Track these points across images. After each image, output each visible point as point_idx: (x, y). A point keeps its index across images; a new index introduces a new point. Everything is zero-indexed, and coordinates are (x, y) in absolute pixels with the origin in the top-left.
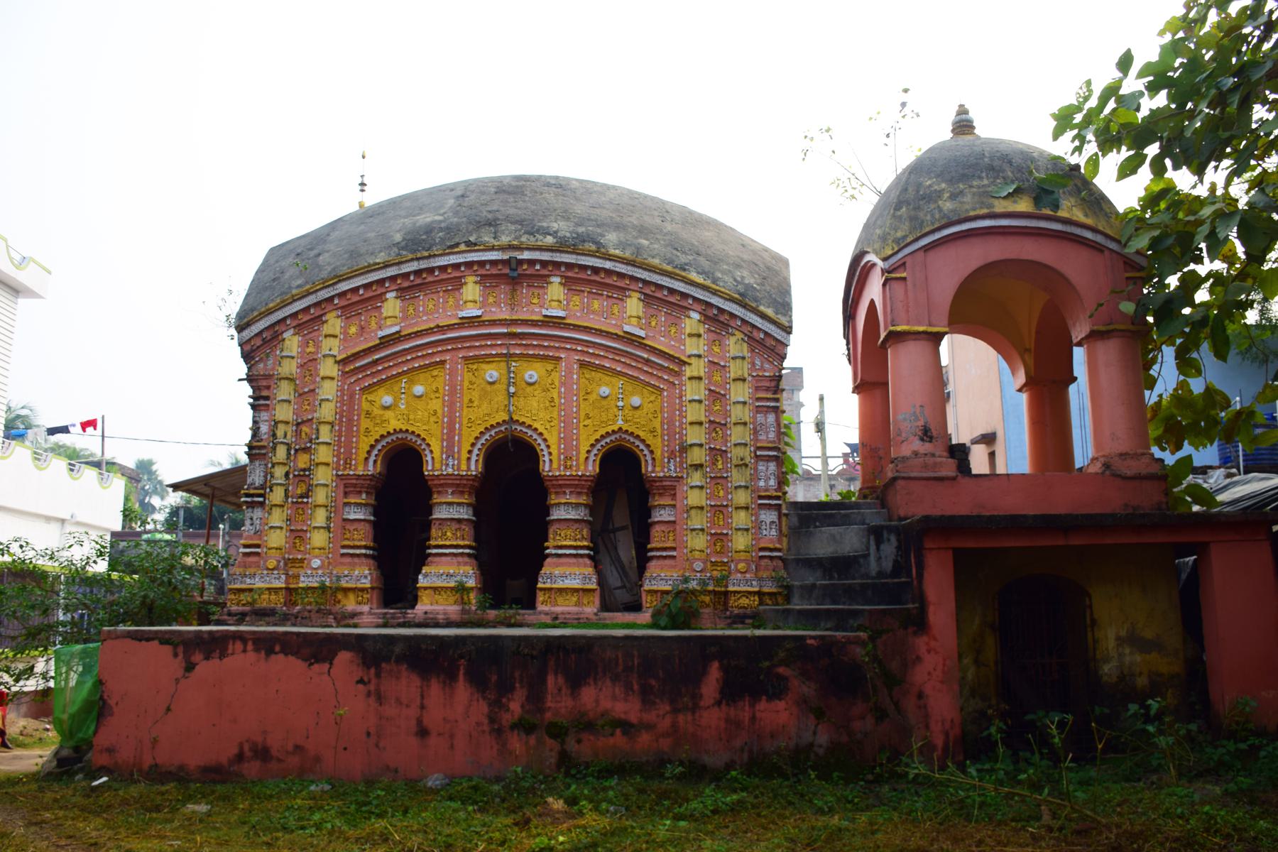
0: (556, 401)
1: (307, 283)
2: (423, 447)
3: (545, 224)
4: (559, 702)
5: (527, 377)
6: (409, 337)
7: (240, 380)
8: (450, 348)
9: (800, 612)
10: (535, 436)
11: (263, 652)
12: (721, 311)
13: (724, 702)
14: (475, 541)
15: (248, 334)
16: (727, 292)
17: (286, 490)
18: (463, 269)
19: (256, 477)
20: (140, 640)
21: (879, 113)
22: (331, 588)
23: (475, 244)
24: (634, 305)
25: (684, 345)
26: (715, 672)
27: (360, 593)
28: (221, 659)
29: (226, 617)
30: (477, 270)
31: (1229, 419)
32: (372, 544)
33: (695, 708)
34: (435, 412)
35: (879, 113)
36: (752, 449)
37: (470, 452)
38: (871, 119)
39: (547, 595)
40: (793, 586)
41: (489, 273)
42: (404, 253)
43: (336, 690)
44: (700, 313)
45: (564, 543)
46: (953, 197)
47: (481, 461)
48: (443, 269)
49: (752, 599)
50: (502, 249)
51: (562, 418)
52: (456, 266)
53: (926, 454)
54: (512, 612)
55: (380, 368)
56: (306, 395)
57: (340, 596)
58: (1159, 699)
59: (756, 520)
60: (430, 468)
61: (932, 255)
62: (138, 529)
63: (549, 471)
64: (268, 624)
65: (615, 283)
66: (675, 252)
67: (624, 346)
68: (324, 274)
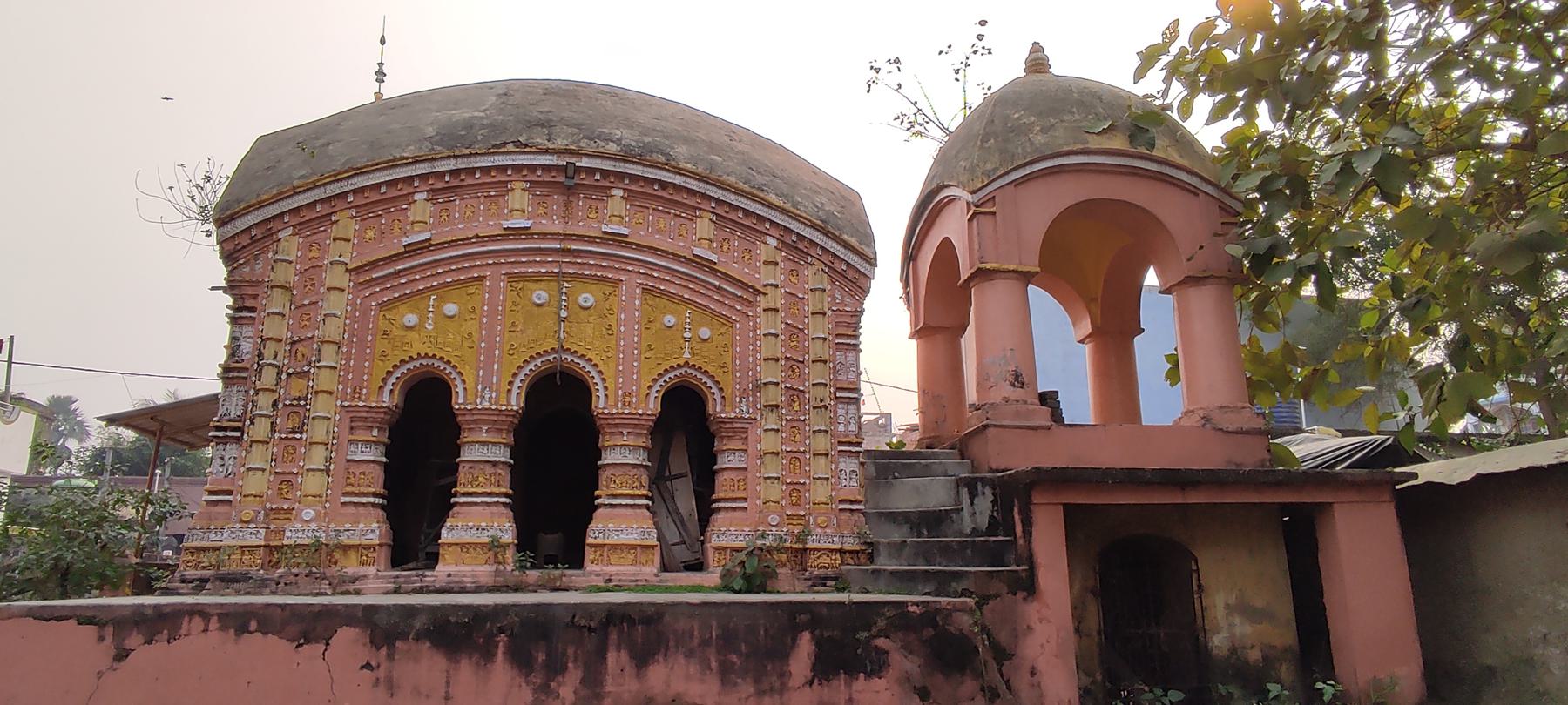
0: (614, 328)
1: (313, 174)
2: (452, 377)
3: (606, 130)
4: (621, 685)
5: (581, 300)
6: (440, 246)
7: (213, 288)
8: (491, 262)
9: (892, 572)
10: (593, 373)
11: (232, 631)
12: (801, 237)
13: (816, 681)
14: (393, 541)
15: (231, 229)
16: (809, 217)
17: (272, 423)
18: (509, 172)
19: (233, 407)
20: (48, 620)
21: (950, 47)
22: (327, 545)
23: (526, 146)
24: (704, 226)
25: (759, 273)
26: (805, 646)
27: (365, 552)
28: (169, 643)
29: (177, 584)
30: (526, 175)
31: (1430, 366)
32: (382, 491)
33: (783, 689)
34: (470, 335)
35: (950, 47)
36: (832, 390)
37: (511, 383)
38: (941, 53)
39: (599, 552)
40: (879, 543)
41: (540, 179)
42: (439, 148)
43: (332, 678)
44: (777, 239)
45: (620, 492)
46: (1044, 130)
47: (523, 394)
48: (486, 170)
49: (833, 557)
50: (557, 153)
51: (621, 349)
52: (502, 169)
53: (1017, 401)
54: (557, 572)
55: (403, 281)
56: (304, 310)
57: (337, 555)
58: (1332, 683)
59: (836, 468)
60: (461, 401)
61: (1023, 191)
62: (47, 475)
63: (604, 408)
64: (238, 593)
65: (685, 201)
66: (750, 171)
67: (693, 271)
68: (337, 166)
